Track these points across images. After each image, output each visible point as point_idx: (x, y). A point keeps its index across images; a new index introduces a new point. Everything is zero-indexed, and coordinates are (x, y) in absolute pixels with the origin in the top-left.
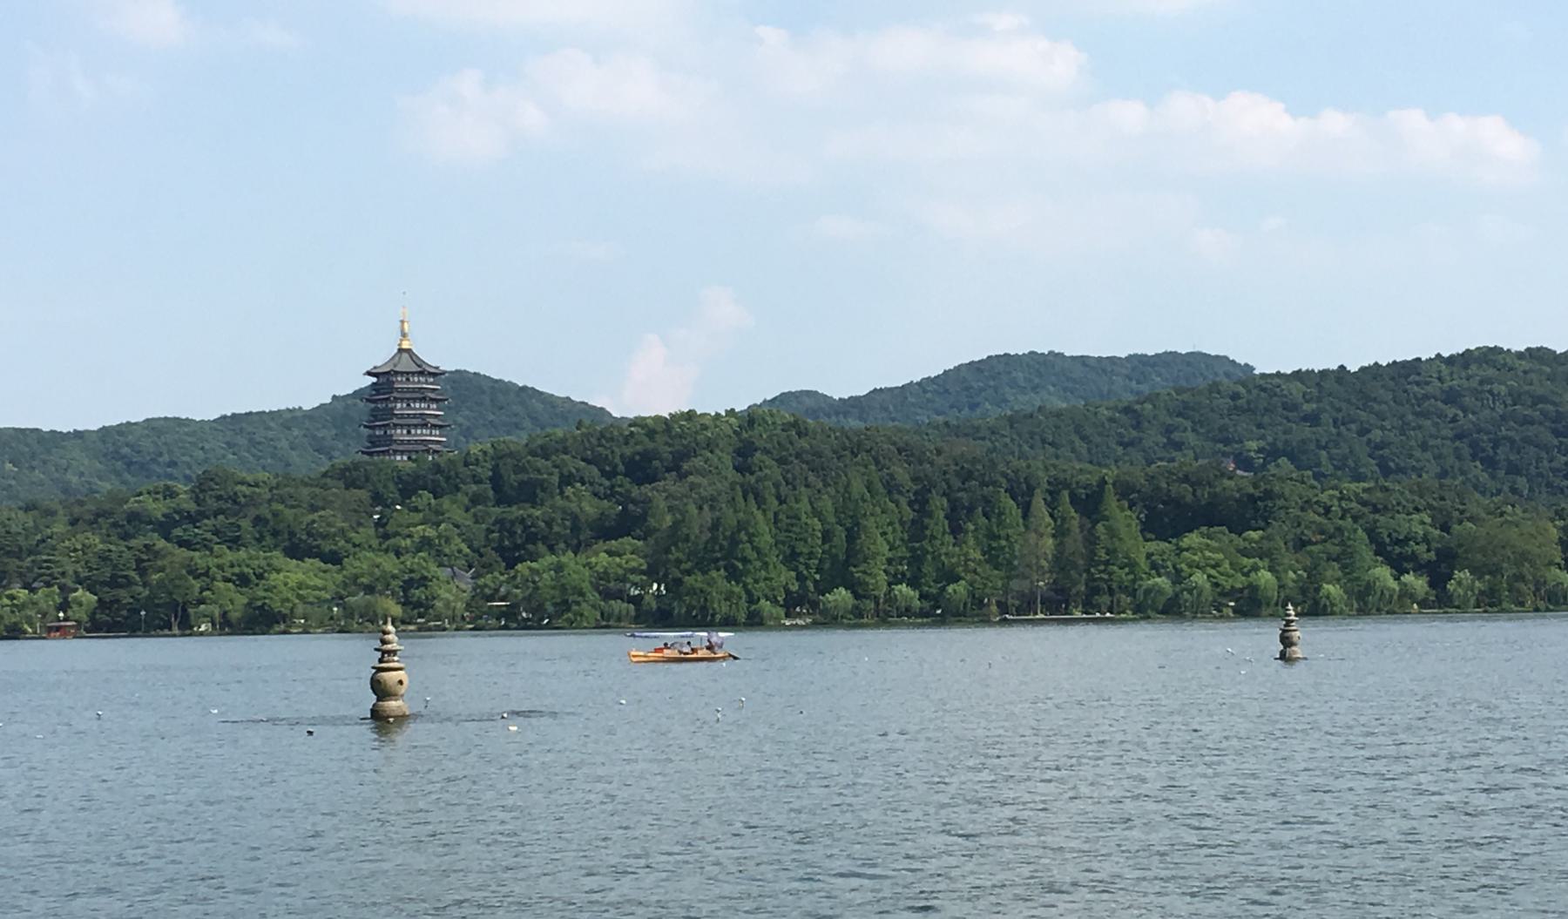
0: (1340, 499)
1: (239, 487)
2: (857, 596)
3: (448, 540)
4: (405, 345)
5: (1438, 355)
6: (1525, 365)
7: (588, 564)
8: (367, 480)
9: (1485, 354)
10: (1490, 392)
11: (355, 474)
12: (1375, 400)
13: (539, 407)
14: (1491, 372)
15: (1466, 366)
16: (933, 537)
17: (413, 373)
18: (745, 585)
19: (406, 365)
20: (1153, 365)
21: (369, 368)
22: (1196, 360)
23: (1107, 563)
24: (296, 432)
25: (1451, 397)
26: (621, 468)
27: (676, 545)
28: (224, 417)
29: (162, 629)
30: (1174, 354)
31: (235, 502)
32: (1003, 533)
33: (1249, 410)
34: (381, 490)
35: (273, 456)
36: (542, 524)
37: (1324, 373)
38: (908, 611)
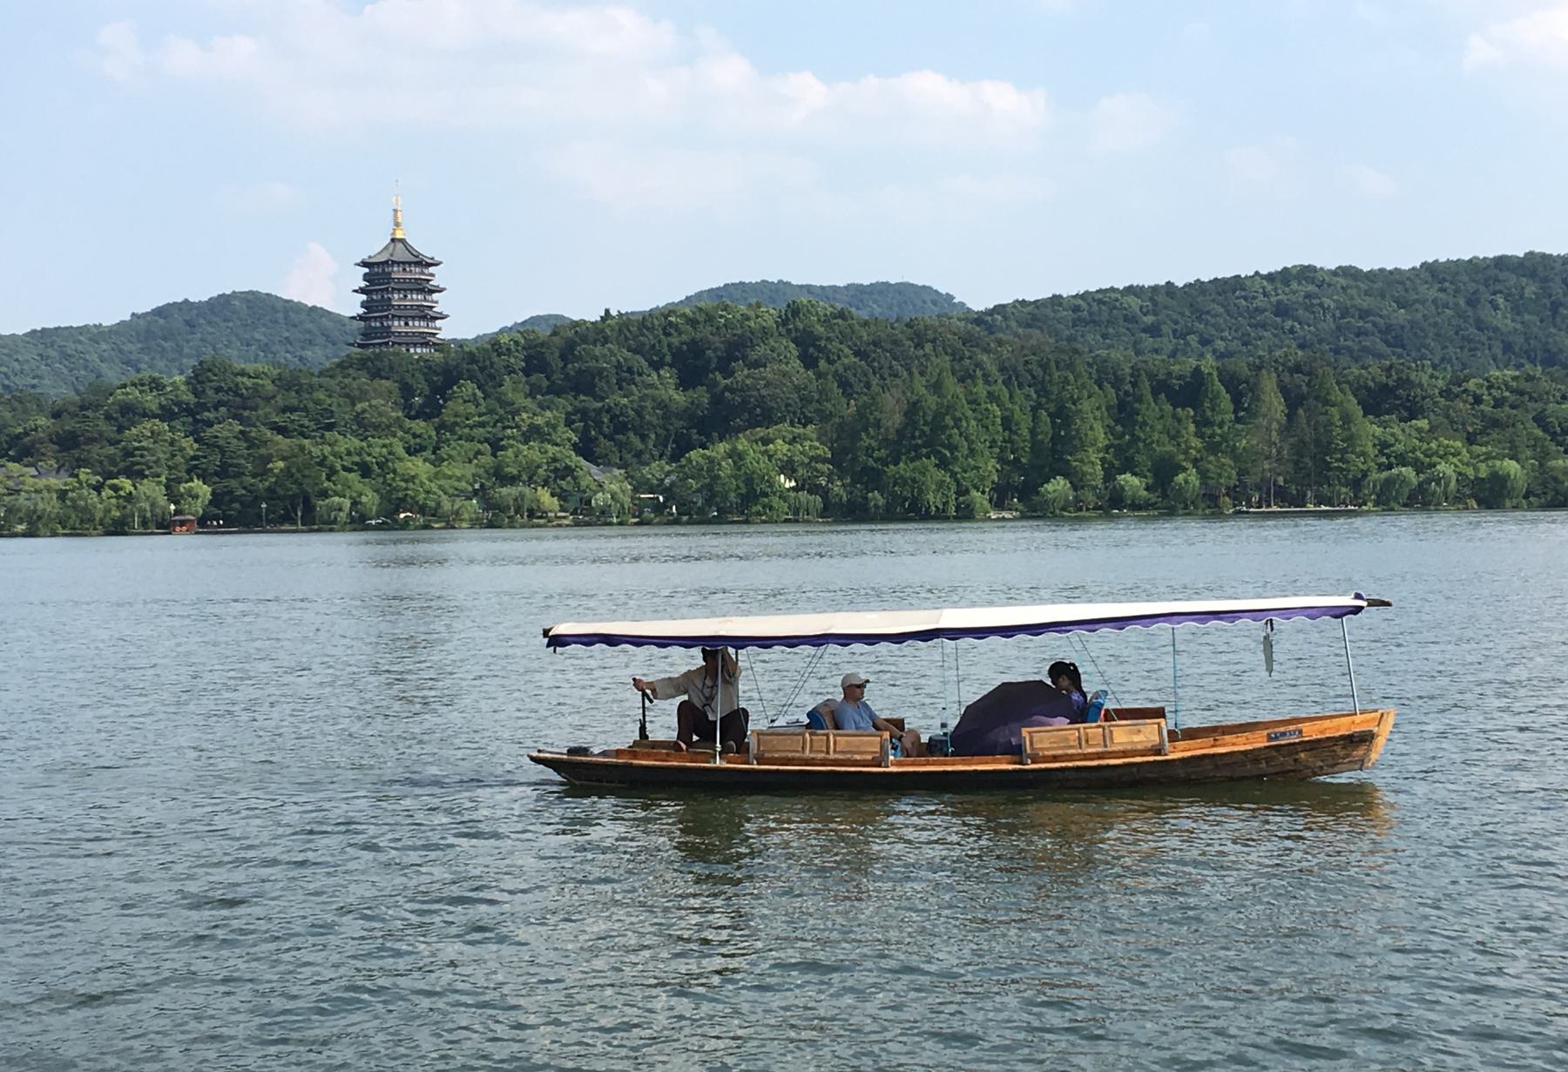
0: (1489, 388)
1: (239, 379)
2: (1075, 488)
3: (554, 427)
4: (399, 235)
5: (1257, 273)
6: (1342, 281)
7: (766, 452)
8: (391, 368)
9: (568, 352)
10: (1321, 305)
11: (377, 363)
12: (1208, 312)
13: (329, 324)
14: (1311, 288)
15: (1287, 283)
16: (1144, 424)
17: (410, 263)
18: (953, 475)
19: (401, 254)
20: (871, 293)
21: (365, 257)
22: (904, 290)
23: (1344, 451)
24: (104, 346)
25: (1282, 311)
26: (668, 359)
27: (866, 431)
28: (34, 331)
29: (282, 524)
30: (887, 284)
31: (237, 394)
32: (1218, 419)
33: (1094, 322)
34: (410, 381)
35: (86, 368)
36: (631, 413)
37: (1155, 289)
38: (1135, 507)
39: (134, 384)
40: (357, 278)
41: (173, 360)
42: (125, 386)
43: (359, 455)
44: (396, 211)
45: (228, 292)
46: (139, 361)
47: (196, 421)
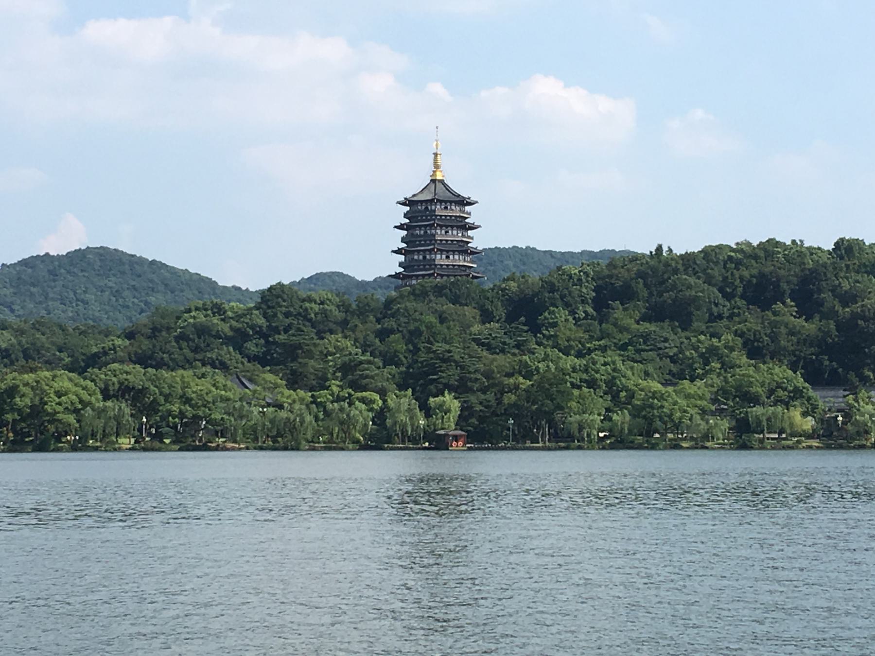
4: (439, 176)
13: (168, 275)
17: (451, 202)
19: (442, 193)
21: (409, 196)
39: (197, 309)
40: (399, 215)
41: (40, 303)
42: (189, 311)
43: (586, 371)
44: (436, 155)
45: (83, 248)
46: (12, 303)
47: (267, 342)
